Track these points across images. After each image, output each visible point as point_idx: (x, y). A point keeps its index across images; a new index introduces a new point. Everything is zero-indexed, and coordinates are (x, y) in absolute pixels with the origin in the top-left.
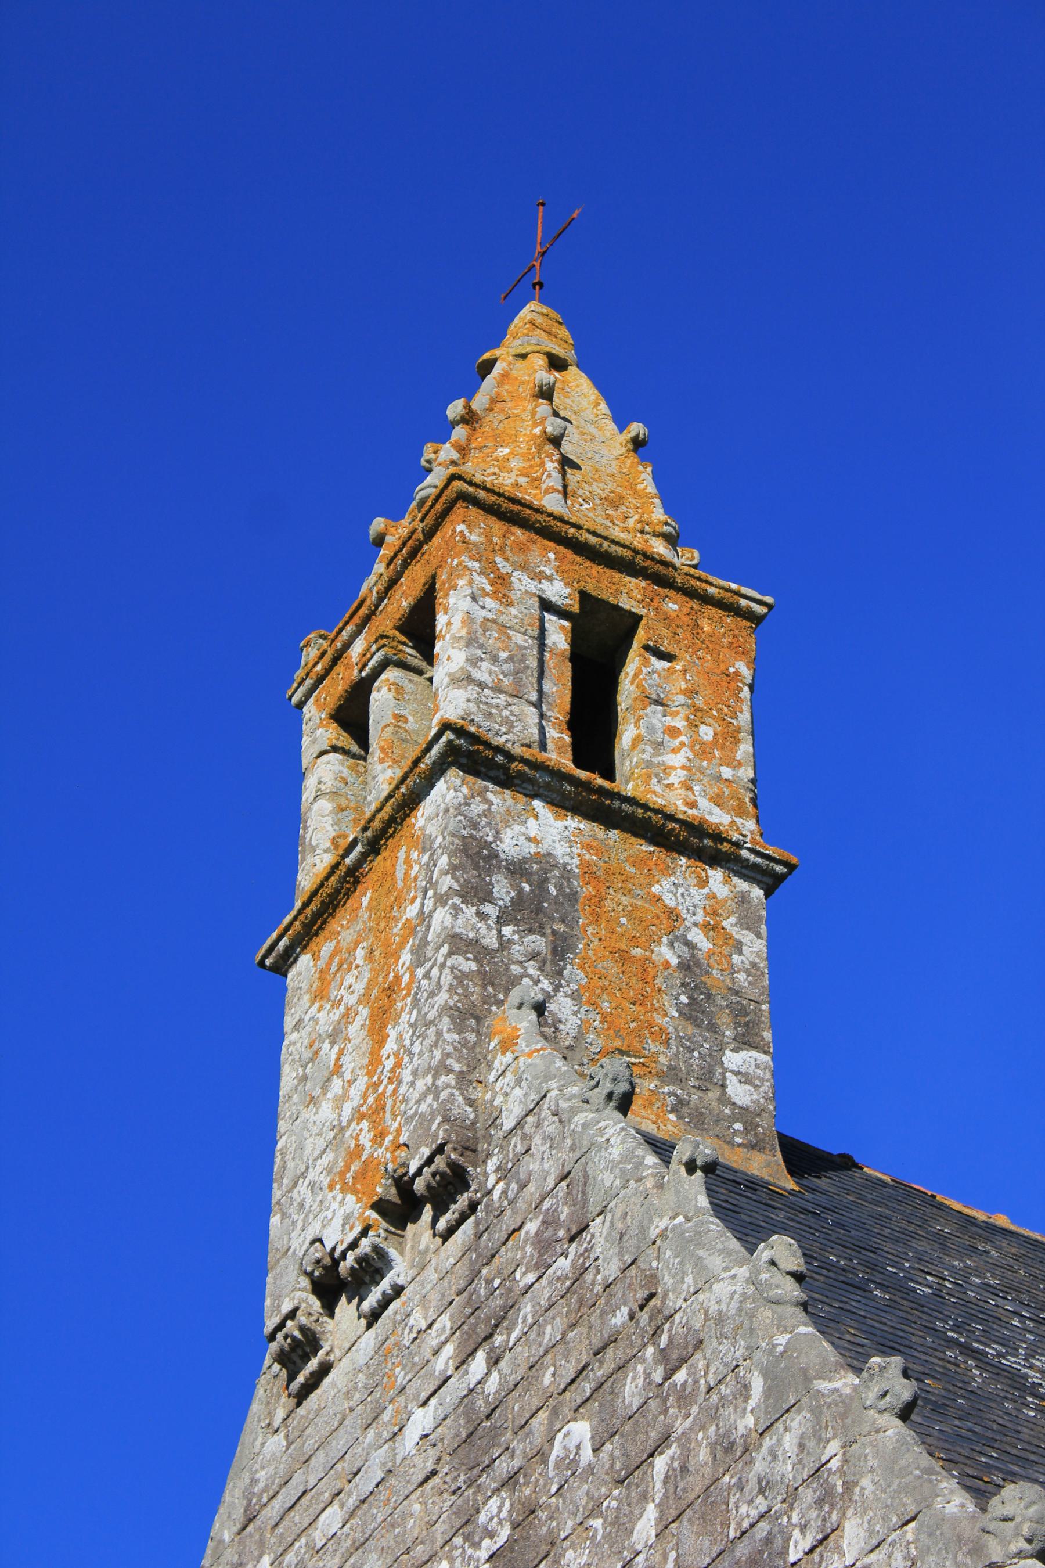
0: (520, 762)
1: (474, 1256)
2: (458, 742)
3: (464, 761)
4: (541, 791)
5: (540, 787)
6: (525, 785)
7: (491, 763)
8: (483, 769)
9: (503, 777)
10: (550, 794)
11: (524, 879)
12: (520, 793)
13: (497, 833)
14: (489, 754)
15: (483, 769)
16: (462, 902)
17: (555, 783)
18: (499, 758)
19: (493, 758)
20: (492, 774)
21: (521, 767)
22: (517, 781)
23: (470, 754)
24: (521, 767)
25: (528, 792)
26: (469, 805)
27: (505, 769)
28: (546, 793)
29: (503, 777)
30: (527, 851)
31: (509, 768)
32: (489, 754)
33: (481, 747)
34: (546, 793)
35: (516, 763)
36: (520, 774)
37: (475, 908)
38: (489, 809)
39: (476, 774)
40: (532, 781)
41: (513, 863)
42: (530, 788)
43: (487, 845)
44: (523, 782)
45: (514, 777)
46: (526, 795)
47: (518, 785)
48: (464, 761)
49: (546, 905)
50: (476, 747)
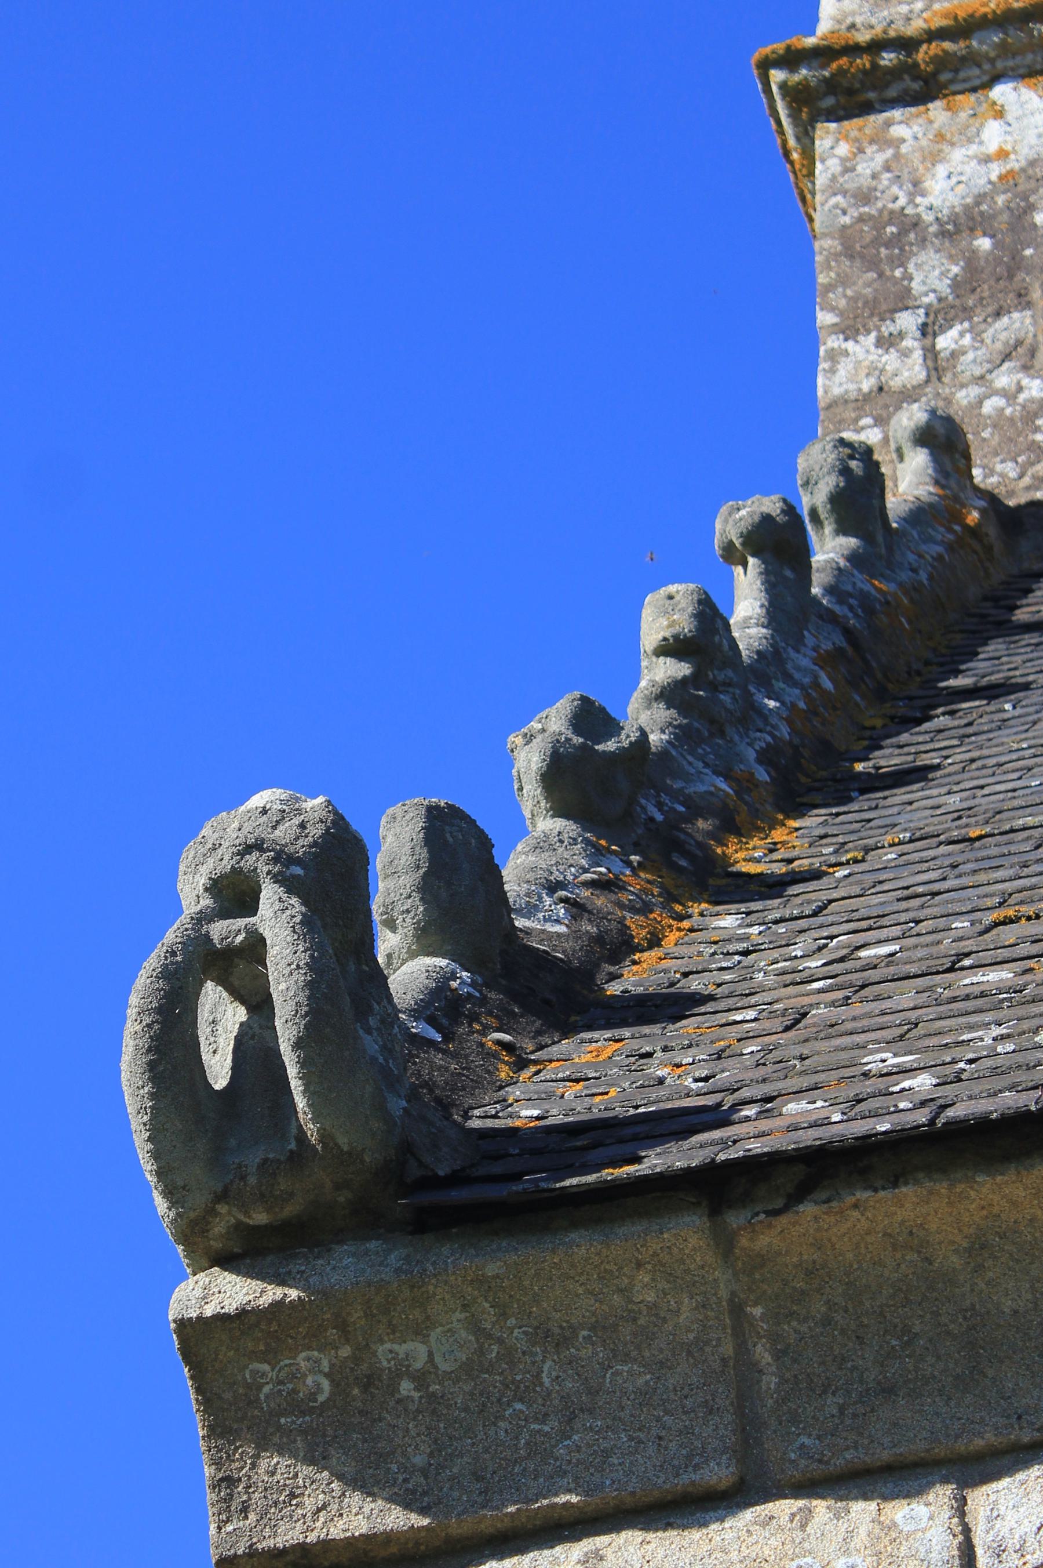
0: (929, 41)
1: (701, 824)
2: (796, 78)
3: (829, 102)
4: (1000, 65)
5: (992, 61)
6: (962, 75)
7: (877, 78)
8: (872, 95)
9: (916, 86)
10: (1018, 60)
11: (979, 233)
12: (962, 92)
13: (916, 183)
14: (864, 62)
15: (872, 95)
16: (846, 339)
17: (1016, 36)
18: (888, 59)
19: (875, 66)
20: (892, 92)
21: (934, 48)
22: (944, 77)
23: (831, 85)
24: (934, 48)
25: (977, 82)
26: (853, 169)
27: (911, 69)
28: (1010, 63)
29: (916, 86)
30: (983, 181)
31: (916, 65)
32: (864, 62)
33: (844, 61)
34: (1010, 63)
35: (924, 47)
36: (942, 62)
37: (873, 335)
38: (897, 156)
39: (866, 109)
40: (971, 59)
41: (954, 219)
42: (976, 71)
43: (897, 216)
44: (956, 71)
45: (935, 74)
46: (974, 90)
47: (951, 81)
48: (829, 102)
49: (1029, 252)
50: (834, 66)
